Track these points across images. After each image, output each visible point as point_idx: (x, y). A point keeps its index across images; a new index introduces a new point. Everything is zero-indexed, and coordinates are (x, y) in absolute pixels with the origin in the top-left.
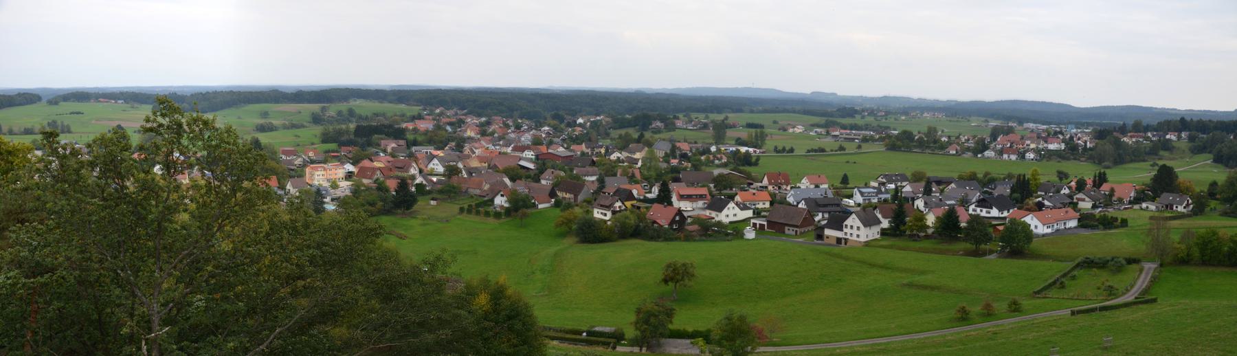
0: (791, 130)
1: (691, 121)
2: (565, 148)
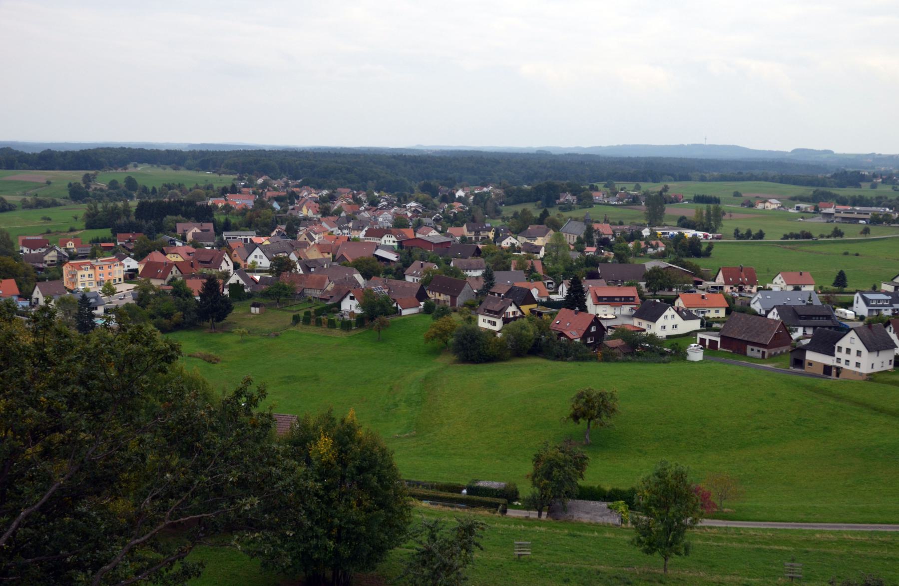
0: (760, 206)
1: (615, 194)
2: (440, 232)
